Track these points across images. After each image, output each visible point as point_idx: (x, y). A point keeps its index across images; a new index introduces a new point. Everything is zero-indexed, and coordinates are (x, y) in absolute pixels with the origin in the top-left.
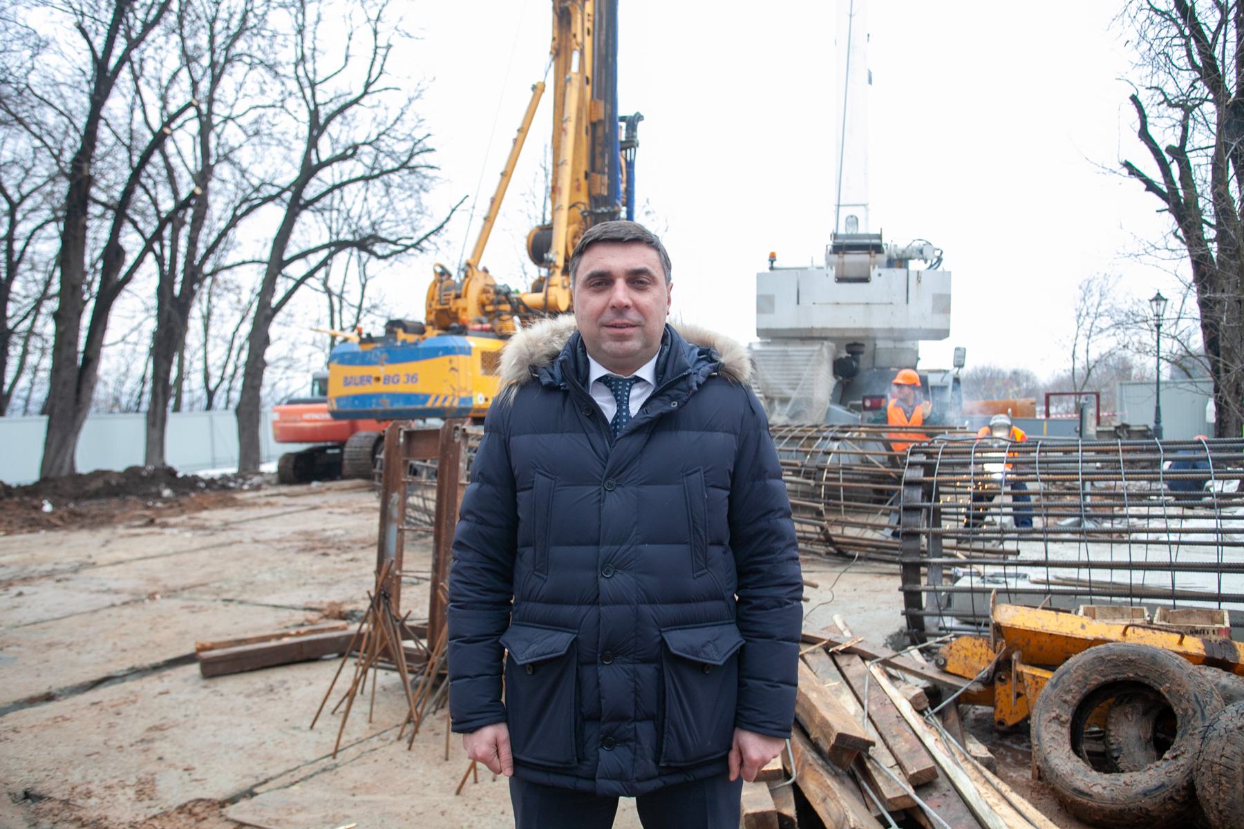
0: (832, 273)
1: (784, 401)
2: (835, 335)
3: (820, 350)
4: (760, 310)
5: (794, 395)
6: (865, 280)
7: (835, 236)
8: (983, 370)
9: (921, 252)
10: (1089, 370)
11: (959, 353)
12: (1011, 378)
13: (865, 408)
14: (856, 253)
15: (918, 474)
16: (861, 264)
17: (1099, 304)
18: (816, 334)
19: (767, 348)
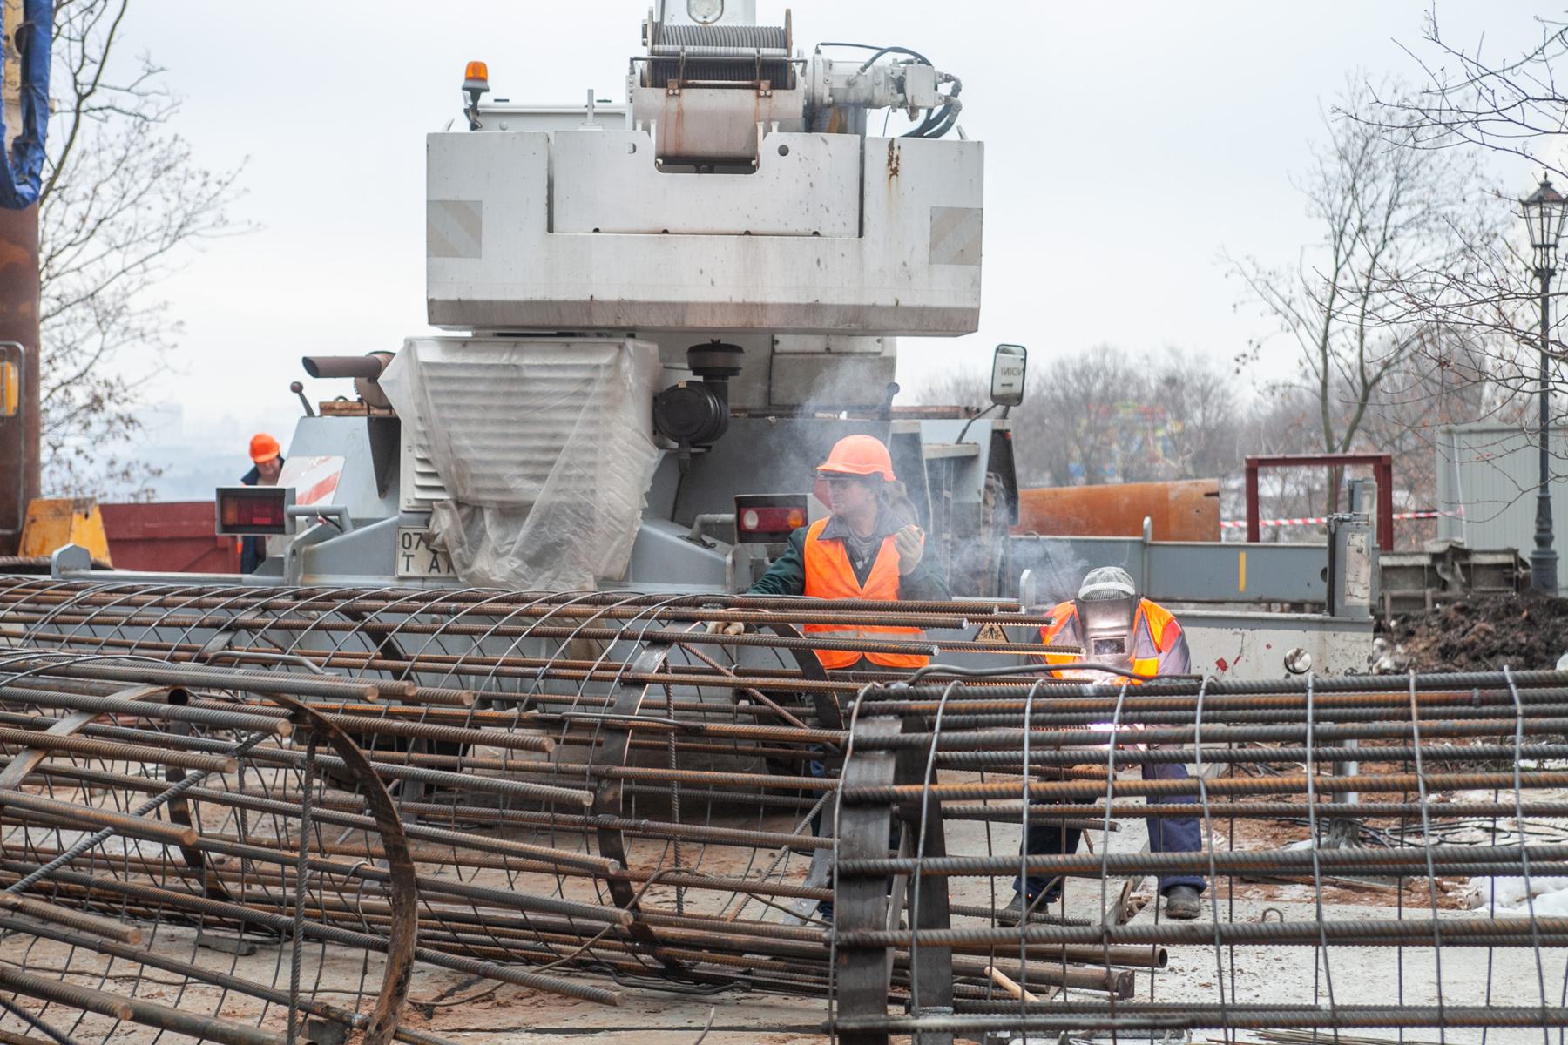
0: (649, 144)
1: (512, 512)
2: (655, 320)
3: (615, 366)
4: (437, 246)
5: (540, 495)
6: (743, 164)
7: (656, 32)
8: (1083, 373)
9: (900, 85)
10: (1367, 388)
11: (1007, 361)
12: (1159, 396)
13: (745, 536)
14: (716, 88)
15: (877, 775)
16: (732, 117)
17: (1393, 204)
18: (600, 321)
19: (459, 358)
